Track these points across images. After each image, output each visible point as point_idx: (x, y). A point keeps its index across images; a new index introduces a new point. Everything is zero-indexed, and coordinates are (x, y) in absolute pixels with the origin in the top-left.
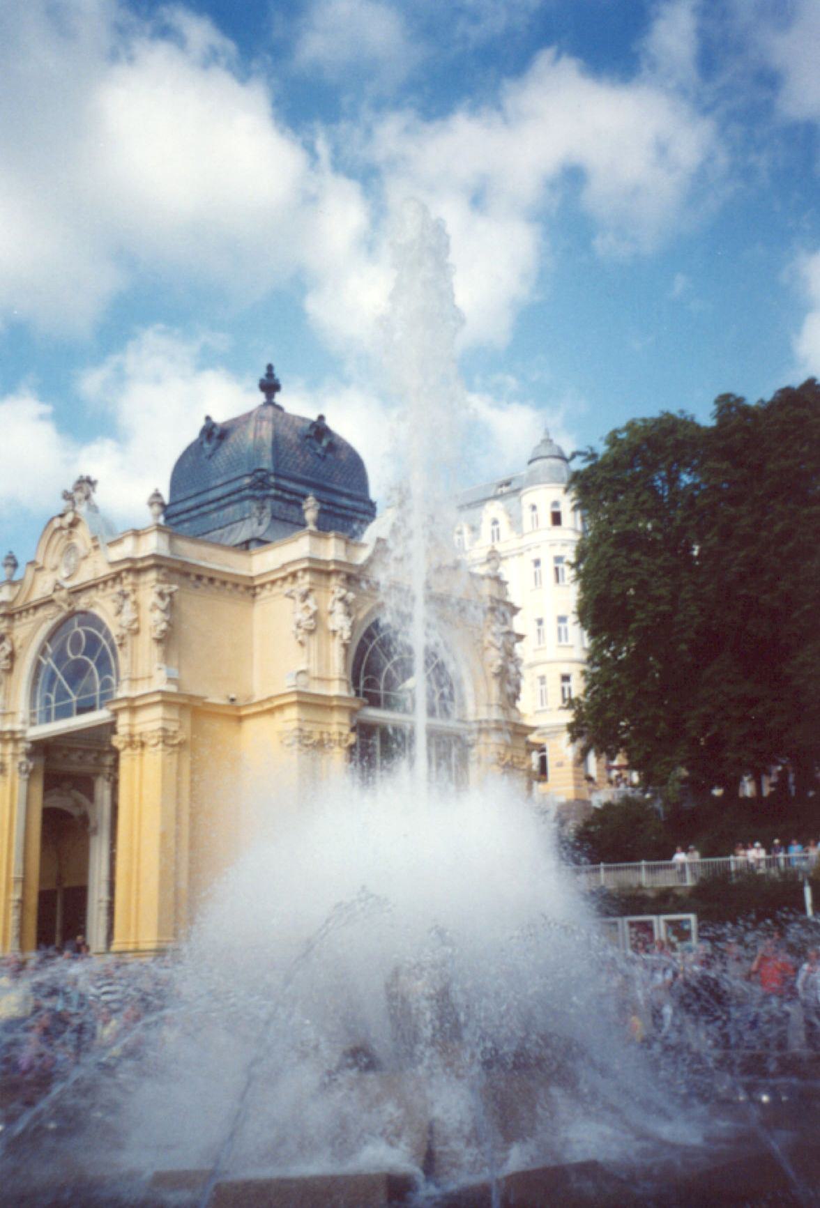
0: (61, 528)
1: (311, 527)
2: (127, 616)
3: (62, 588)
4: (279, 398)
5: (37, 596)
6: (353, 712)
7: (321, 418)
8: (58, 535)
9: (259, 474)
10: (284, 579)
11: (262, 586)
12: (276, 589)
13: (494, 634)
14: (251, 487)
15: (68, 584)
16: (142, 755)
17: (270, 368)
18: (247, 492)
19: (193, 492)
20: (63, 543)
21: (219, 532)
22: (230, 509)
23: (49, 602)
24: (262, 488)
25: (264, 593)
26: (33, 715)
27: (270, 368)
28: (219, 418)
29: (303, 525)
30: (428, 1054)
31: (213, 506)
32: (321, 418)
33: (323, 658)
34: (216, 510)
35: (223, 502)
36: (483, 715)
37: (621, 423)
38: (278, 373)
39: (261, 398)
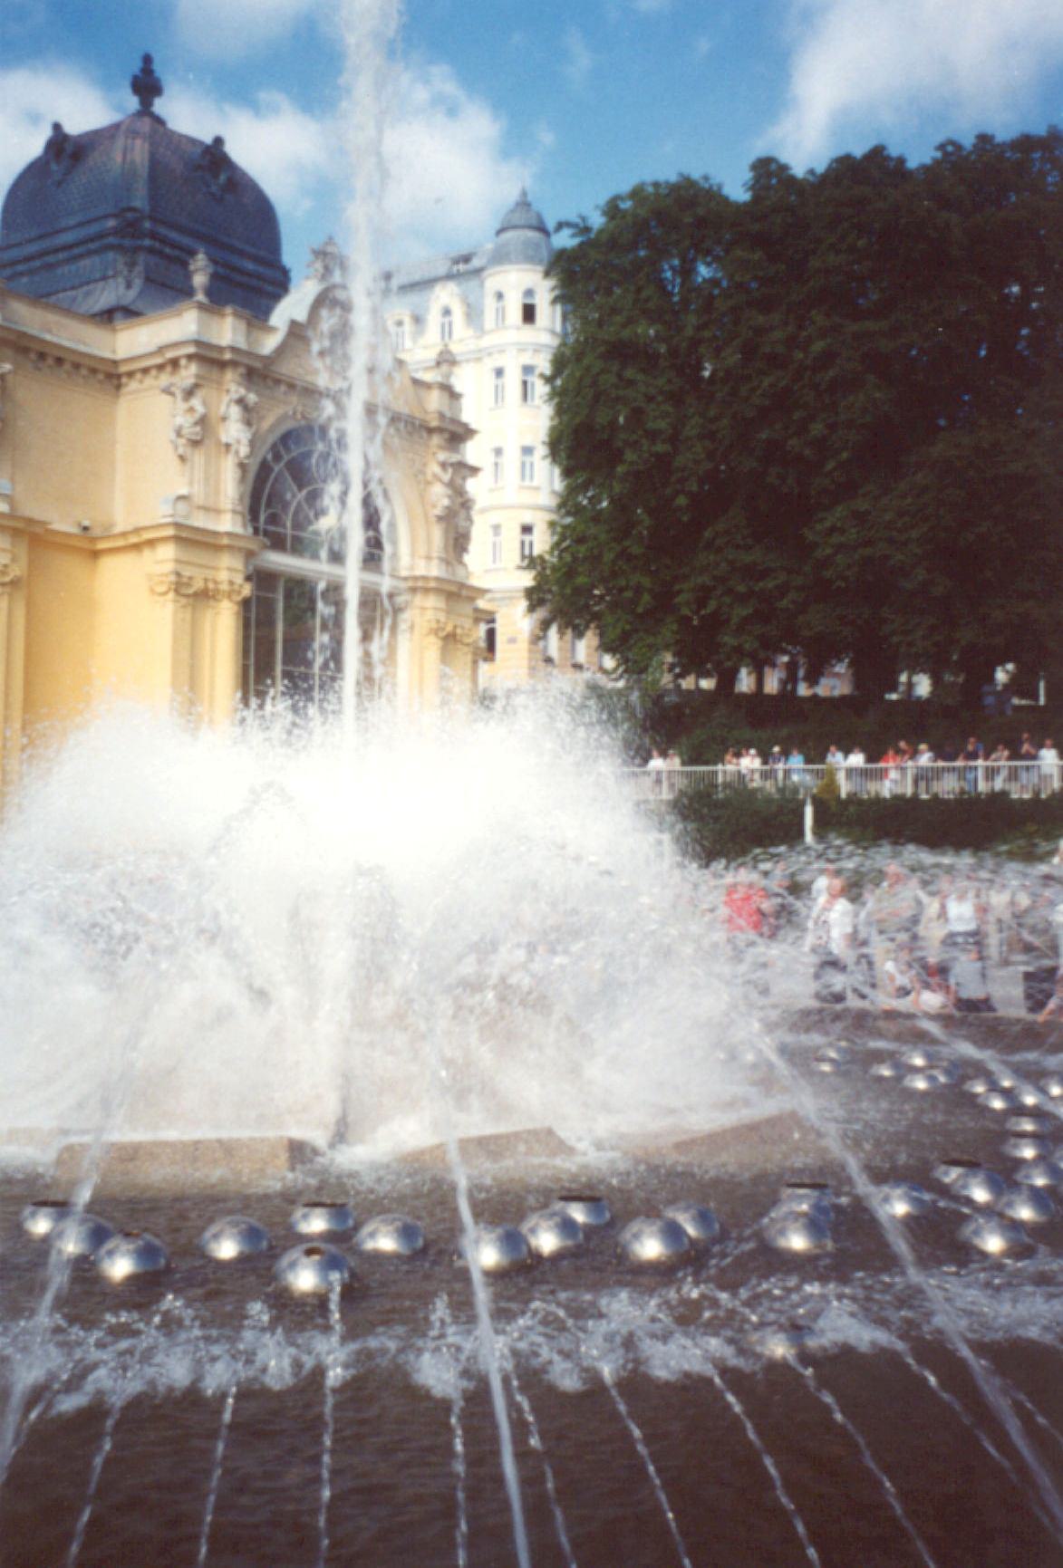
1: (200, 297)
4: (159, 106)
6: (249, 555)
13: (444, 465)
22: (86, 262)
27: (147, 60)
28: (74, 127)
33: (212, 481)
36: (421, 569)
39: (133, 103)
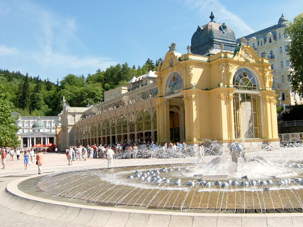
27: (212, 13)
38: (214, 14)
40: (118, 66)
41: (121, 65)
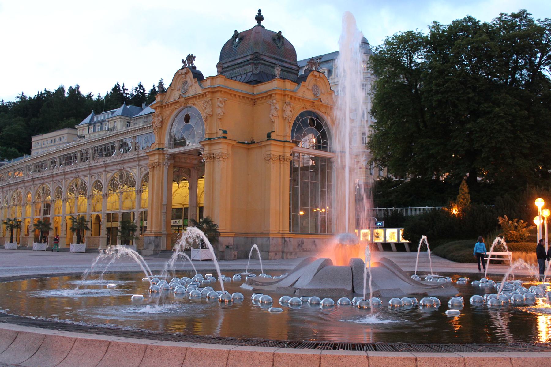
0: (182, 74)
2: (208, 110)
3: (182, 97)
4: (262, 23)
5: (172, 100)
7: (280, 32)
8: (180, 77)
9: (256, 55)
10: (266, 97)
11: (258, 99)
12: (263, 101)
13: (221, 102)
14: (252, 59)
15: (184, 96)
16: (213, 161)
17: (260, 11)
18: (251, 61)
19: (230, 59)
20: (182, 81)
21: (301, 158)
23: (177, 102)
24: (257, 60)
25: (258, 102)
26: (170, 144)
27: (260, 11)
29: (274, 77)
30: (488, 298)
31: (237, 66)
32: (280, 32)
34: (238, 68)
35: (241, 65)
37: (391, 35)
38: (262, 13)
39: (256, 23)
40: (61, 91)
41: (67, 90)
